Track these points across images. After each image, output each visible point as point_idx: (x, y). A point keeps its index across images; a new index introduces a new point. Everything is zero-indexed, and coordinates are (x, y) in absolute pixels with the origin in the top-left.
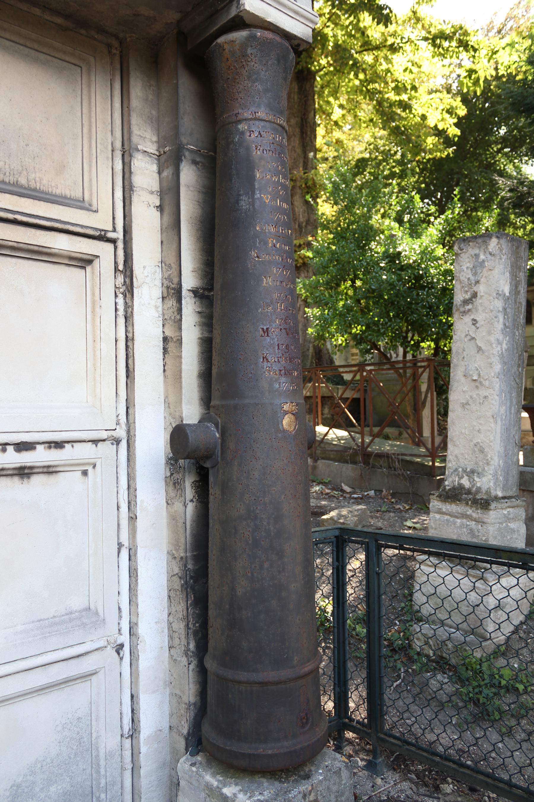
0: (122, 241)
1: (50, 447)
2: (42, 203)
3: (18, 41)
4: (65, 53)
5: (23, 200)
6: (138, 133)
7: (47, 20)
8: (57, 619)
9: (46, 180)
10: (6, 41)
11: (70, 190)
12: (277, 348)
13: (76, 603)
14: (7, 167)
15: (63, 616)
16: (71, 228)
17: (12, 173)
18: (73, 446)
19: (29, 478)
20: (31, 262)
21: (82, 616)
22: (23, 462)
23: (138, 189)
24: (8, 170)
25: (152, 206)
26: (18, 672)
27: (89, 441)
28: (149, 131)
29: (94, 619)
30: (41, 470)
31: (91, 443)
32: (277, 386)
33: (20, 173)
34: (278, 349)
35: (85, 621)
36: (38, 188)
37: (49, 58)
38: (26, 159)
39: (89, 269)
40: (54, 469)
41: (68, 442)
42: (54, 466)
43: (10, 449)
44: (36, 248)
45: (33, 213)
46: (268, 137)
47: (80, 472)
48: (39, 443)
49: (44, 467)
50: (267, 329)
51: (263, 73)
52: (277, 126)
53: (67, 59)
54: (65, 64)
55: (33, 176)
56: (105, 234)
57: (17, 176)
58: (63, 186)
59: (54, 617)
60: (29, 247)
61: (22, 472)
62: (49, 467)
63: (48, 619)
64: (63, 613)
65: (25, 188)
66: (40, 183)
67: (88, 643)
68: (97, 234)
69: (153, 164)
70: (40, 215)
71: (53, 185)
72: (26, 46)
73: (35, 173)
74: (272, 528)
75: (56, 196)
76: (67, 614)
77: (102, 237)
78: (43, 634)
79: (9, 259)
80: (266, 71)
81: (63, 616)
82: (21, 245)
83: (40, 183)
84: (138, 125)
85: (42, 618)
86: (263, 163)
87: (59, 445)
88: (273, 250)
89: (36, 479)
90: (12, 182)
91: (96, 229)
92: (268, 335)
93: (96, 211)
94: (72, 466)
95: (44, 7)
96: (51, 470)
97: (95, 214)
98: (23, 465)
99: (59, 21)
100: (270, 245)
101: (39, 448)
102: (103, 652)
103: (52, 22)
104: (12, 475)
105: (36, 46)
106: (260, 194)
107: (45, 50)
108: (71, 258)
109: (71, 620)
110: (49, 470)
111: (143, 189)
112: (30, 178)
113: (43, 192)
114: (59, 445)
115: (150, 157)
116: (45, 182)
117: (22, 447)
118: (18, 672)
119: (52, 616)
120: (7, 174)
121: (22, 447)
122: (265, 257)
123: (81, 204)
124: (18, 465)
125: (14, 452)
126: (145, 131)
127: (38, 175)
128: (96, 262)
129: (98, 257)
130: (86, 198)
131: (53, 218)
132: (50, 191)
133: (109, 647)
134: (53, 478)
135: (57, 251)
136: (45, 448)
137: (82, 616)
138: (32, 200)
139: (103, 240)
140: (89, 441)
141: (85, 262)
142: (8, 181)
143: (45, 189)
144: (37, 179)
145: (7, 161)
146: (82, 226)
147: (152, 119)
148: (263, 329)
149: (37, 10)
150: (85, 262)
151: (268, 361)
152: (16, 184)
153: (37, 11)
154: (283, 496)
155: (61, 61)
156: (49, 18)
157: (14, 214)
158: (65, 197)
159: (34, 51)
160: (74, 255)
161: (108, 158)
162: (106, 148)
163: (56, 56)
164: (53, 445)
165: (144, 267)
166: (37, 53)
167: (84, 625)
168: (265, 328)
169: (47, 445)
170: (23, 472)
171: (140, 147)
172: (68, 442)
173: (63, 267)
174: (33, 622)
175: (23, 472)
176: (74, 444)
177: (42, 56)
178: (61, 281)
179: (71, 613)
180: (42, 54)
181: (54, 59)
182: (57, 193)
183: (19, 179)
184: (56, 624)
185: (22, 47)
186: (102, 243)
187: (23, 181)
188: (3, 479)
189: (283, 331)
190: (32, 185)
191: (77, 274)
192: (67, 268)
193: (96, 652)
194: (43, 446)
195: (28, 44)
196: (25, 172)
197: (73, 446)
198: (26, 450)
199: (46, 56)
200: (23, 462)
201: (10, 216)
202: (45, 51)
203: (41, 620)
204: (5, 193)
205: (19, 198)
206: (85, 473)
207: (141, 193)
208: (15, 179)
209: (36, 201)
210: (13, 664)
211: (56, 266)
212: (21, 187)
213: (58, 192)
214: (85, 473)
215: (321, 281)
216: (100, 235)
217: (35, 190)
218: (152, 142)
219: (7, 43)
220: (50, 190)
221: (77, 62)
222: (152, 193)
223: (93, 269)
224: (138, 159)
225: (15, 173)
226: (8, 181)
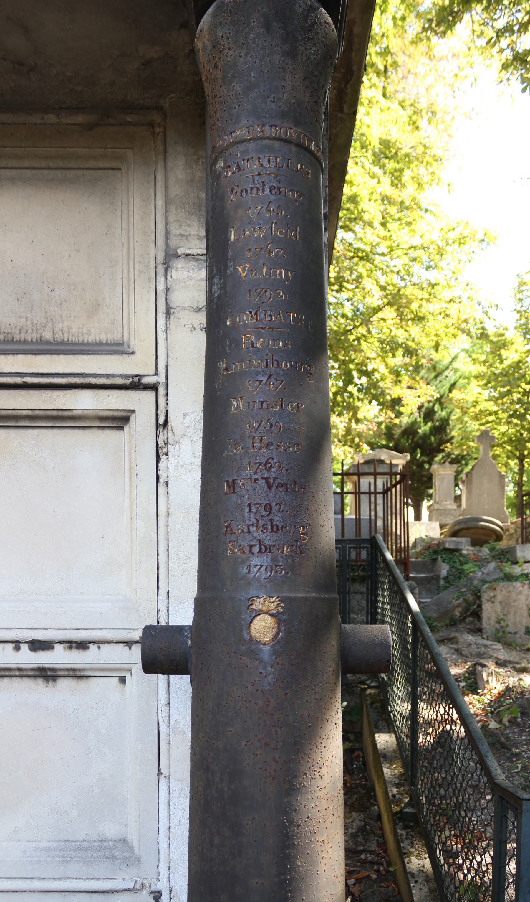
0: (164, 385)
1: (71, 648)
2: (62, 357)
3: (39, 166)
4: (95, 158)
5: (39, 358)
6: (178, 232)
7: (67, 124)
8: (86, 844)
9: (77, 326)
10: (26, 171)
11: (106, 333)
12: (247, 510)
13: (111, 830)
14: (29, 322)
15: (95, 842)
16: (93, 381)
17: (35, 329)
18: (99, 647)
19: (54, 681)
20: (55, 431)
21: (116, 847)
22: (46, 663)
23: (176, 311)
24: (30, 326)
25: (198, 329)
26: (34, 891)
27: (118, 642)
28: (195, 224)
29: (127, 854)
30: (66, 673)
31: (122, 645)
32: (245, 570)
33: (45, 327)
34: (250, 511)
35: (116, 853)
36: (66, 340)
37: (80, 172)
38: (52, 308)
39: (126, 428)
40: (82, 673)
41: (94, 642)
42: (83, 670)
43: (25, 647)
44: (54, 413)
45: (50, 372)
46: (269, 163)
47: (117, 679)
48: (55, 642)
49: (68, 670)
50: (234, 481)
51: (242, 60)
52: (270, 142)
53: (101, 165)
54: (100, 172)
55: (60, 326)
56: (139, 380)
57: (40, 332)
58: (96, 332)
59: (84, 841)
60: (46, 413)
61: (44, 674)
62: (74, 670)
63: (77, 841)
64: (95, 839)
65: (51, 344)
66: (69, 333)
67: (118, 880)
68: (128, 381)
69: (200, 269)
70: (59, 372)
71: (84, 332)
72: (49, 168)
73: (62, 321)
74: (226, 789)
75: (88, 344)
76: (100, 841)
77: (136, 384)
78: (64, 857)
79: (30, 431)
80: (246, 55)
81: (95, 842)
82: (37, 412)
83: (69, 333)
84: (177, 221)
85: (71, 839)
86: (240, 212)
87: (82, 645)
88: (249, 352)
89: (63, 684)
90: (34, 340)
91: (127, 376)
92: (234, 492)
93: (133, 353)
94: (106, 671)
95: (61, 108)
96: (78, 673)
97: (131, 356)
98: (41, 665)
99: (80, 119)
100: (244, 346)
101: (58, 648)
102: (136, 895)
103: (74, 124)
104: (35, 676)
105: (61, 164)
106: (234, 266)
107: (72, 164)
108: (102, 419)
109: (101, 849)
110: (77, 674)
111: (184, 308)
112: (56, 329)
113: (73, 344)
114: (82, 645)
115: (197, 260)
116: (74, 330)
117: (37, 645)
118: (34, 891)
119: (81, 839)
120: (30, 331)
121: (37, 645)
122: (237, 367)
123: (118, 348)
124: (35, 666)
125: (29, 651)
126: (189, 226)
127: (65, 324)
128: (133, 419)
129: (133, 411)
130: (126, 339)
131: (76, 372)
132: (81, 340)
133: (145, 892)
134: (83, 684)
135: (80, 412)
136: (64, 648)
137: (116, 847)
138: (49, 356)
139: (140, 389)
140: (118, 642)
141: (120, 420)
142: (30, 340)
143: (75, 339)
144: (65, 329)
145: (29, 316)
146: (107, 376)
147: (199, 206)
148: (227, 482)
149: (51, 116)
150: (120, 420)
151: (232, 533)
152: (41, 341)
153: (51, 118)
154: (244, 743)
155: (95, 171)
156: (68, 121)
157: (23, 377)
158: (101, 344)
159: (60, 171)
160: (102, 414)
161: (149, 279)
162: (148, 266)
163: (87, 166)
164: (74, 645)
165: (185, 415)
166: (64, 171)
167: (113, 858)
168: (230, 480)
169: (67, 645)
170: (47, 675)
171: (179, 252)
172: (94, 642)
173: (95, 431)
174: (60, 841)
175: (47, 675)
176: (101, 645)
177: (70, 174)
178: (88, 449)
179: (105, 841)
180: (70, 171)
181: (86, 172)
182: (90, 341)
183: (43, 334)
184: (82, 849)
185: (46, 172)
186: (138, 392)
187: (48, 335)
188: (6, 680)
189: (262, 482)
190: (59, 337)
191: (111, 437)
192: (100, 432)
193: (84, 894)
194: (62, 646)
195: (51, 165)
196: (50, 325)
197: (99, 647)
198: (43, 649)
199: (75, 172)
200: (46, 663)
201: (19, 380)
202: (72, 166)
203: (69, 841)
204: (17, 354)
205: (33, 356)
206: (123, 680)
207: (181, 314)
208: (39, 336)
209: (55, 357)
210: (28, 881)
211: (87, 432)
212: (47, 343)
213: (91, 339)
214: (123, 680)
215: (372, 390)
216: (133, 382)
217: (63, 343)
218: (199, 238)
219: (28, 172)
220: (81, 339)
221: (114, 165)
222: (198, 310)
223: (130, 428)
224: (177, 269)
225: (38, 328)
226: (30, 340)
